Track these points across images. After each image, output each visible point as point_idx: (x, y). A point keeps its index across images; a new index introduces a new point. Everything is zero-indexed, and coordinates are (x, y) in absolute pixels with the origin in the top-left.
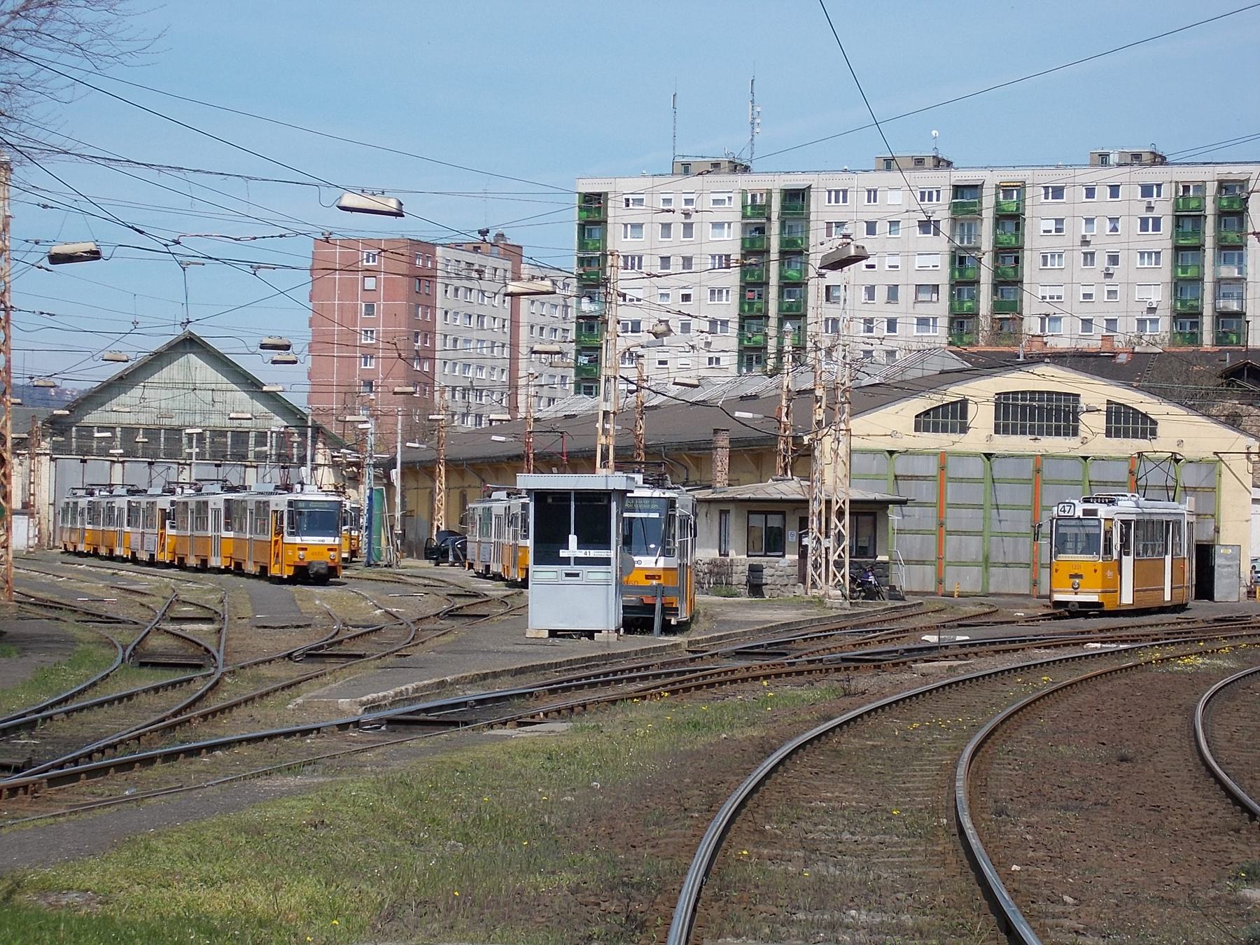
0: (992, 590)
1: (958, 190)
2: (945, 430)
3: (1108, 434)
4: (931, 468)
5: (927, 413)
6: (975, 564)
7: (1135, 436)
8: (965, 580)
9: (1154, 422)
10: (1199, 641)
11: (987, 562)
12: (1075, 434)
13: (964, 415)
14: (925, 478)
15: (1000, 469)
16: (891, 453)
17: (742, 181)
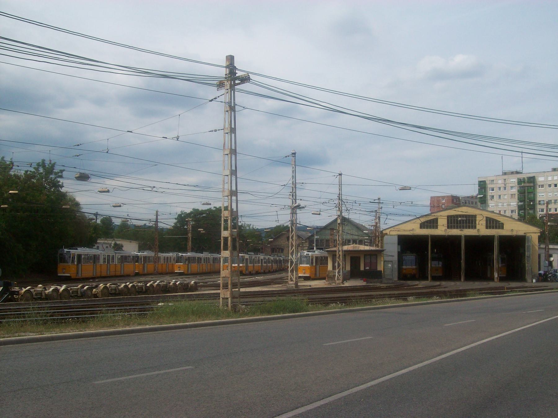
3: (487, 228)
7: (496, 228)
9: (503, 224)
12: (475, 228)
13: (437, 222)
17: (520, 176)
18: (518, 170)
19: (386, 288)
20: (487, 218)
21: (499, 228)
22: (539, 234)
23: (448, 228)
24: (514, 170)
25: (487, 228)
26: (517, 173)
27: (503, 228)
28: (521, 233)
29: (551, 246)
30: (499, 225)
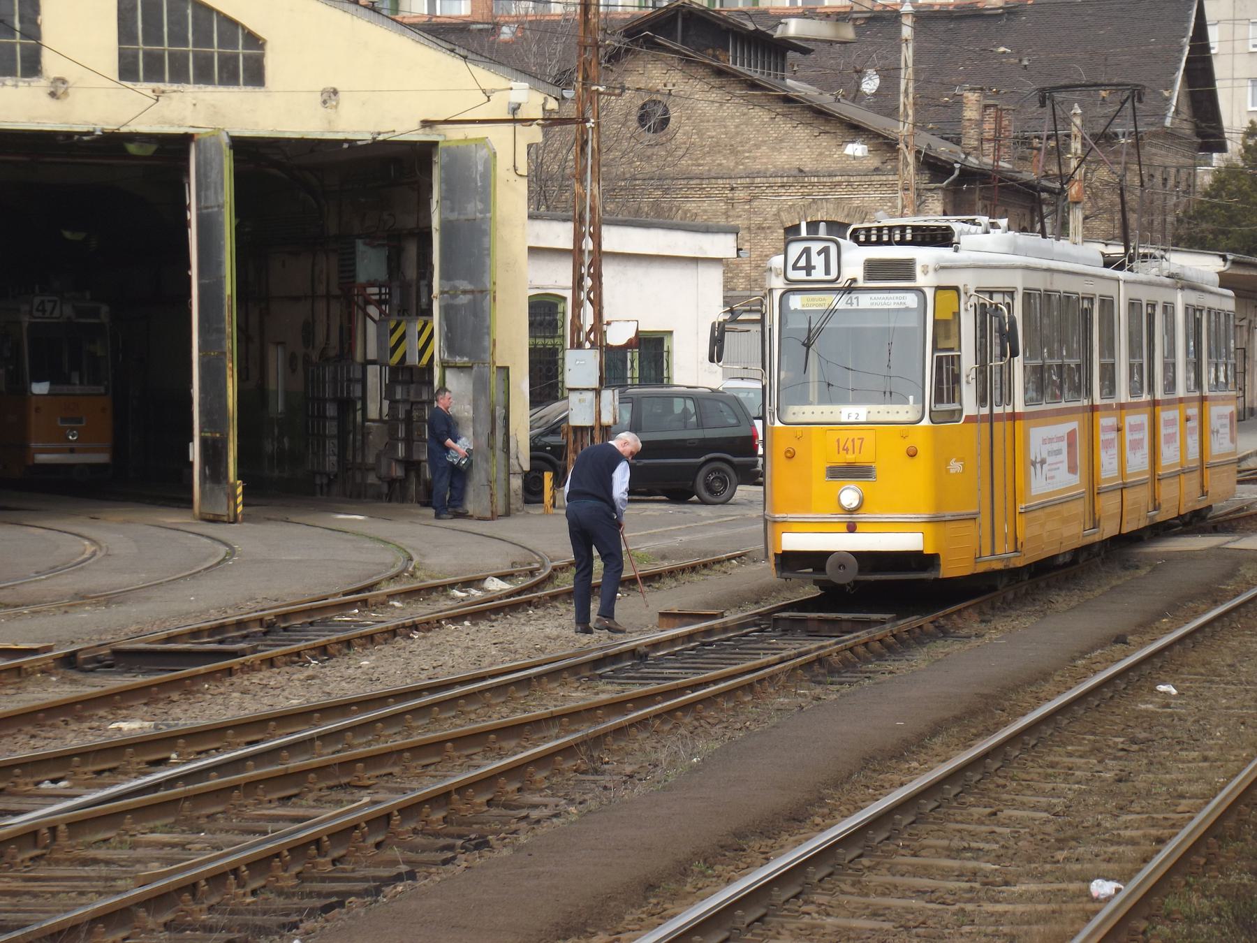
3: (127, 71)
7: (204, 76)
9: (254, 41)
10: (855, 130)
12: (32, 67)
19: (682, 871)
21: (229, 78)
22: (535, 134)
27: (256, 76)
29: (615, 239)
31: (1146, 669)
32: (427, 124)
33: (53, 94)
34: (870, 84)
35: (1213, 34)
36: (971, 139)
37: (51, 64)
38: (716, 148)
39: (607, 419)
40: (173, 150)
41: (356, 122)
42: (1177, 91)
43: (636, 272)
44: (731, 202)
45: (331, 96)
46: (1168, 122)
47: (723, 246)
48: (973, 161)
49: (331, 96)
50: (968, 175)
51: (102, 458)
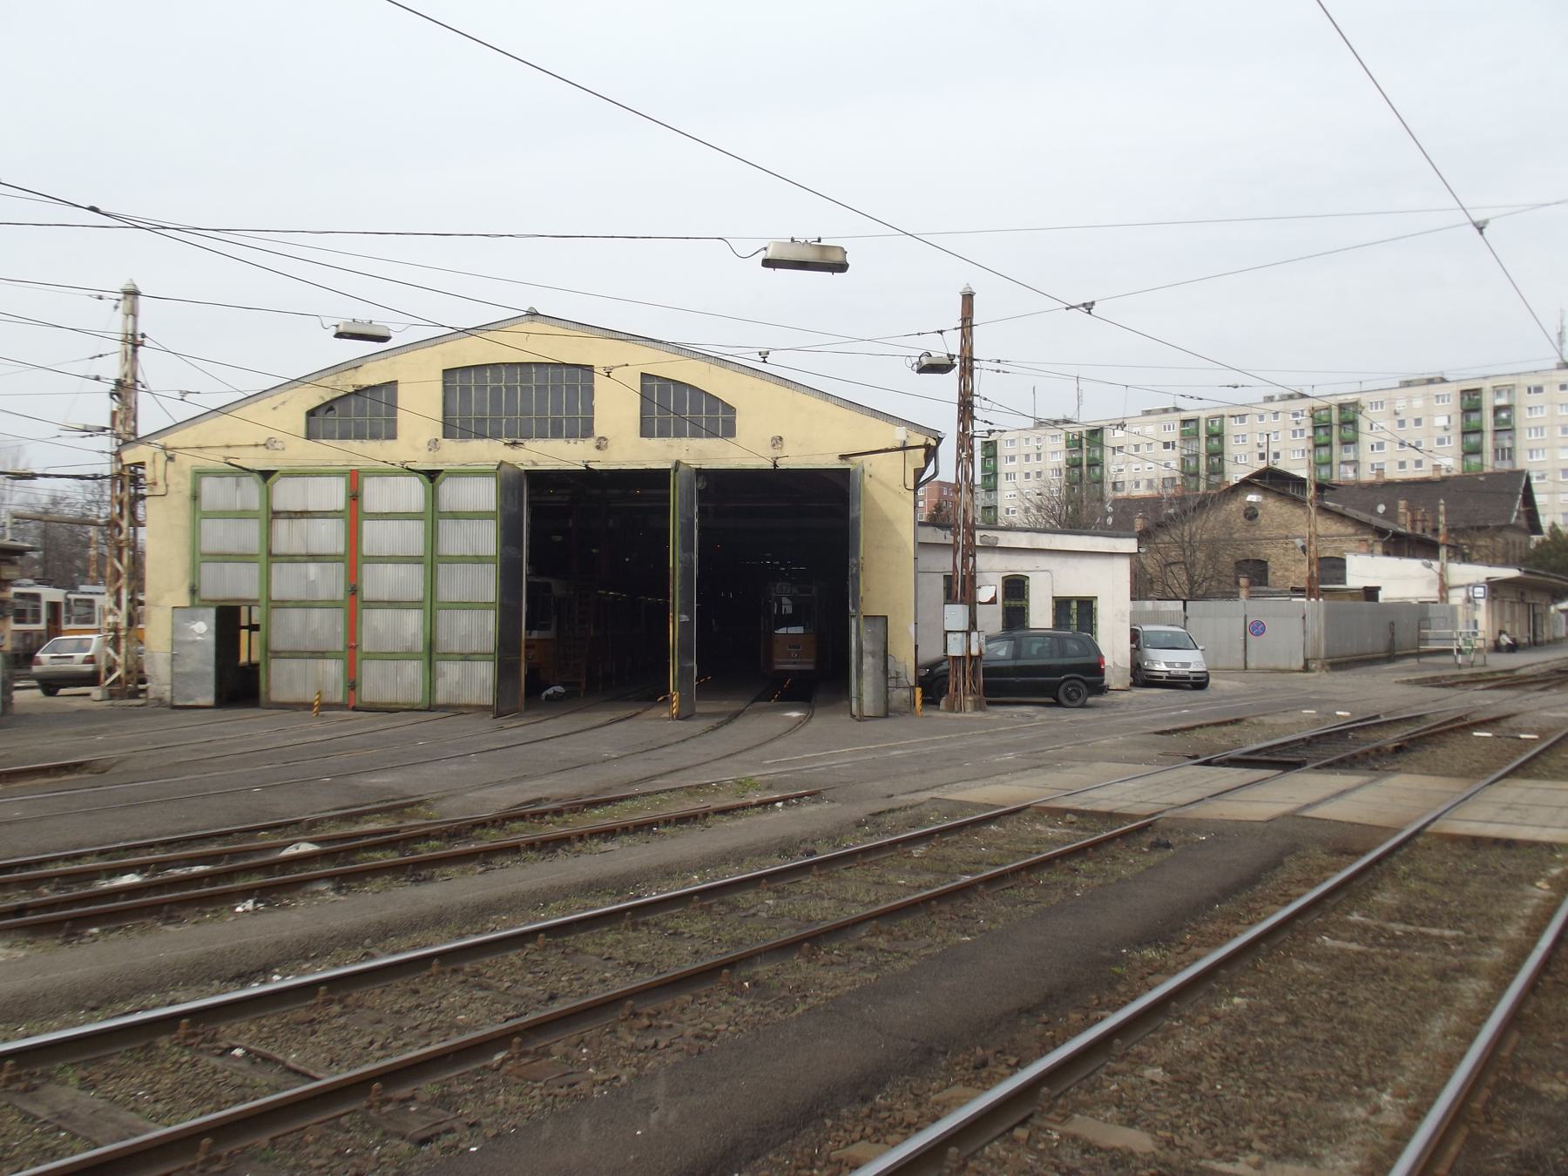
0: (441, 698)
1: (1185, 422)
2: (360, 436)
3: (646, 432)
4: (333, 494)
5: (328, 407)
6: (408, 655)
8: (405, 683)
9: (730, 410)
11: (432, 653)
12: (588, 432)
14: (324, 515)
15: (456, 494)
16: (266, 475)
18: (1069, 416)
20: (645, 376)
23: (447, 434)
24: (1060, 417)
25: (646, 432)
26: (1067, 422)
27: (729, 431)
28: (826, 460)
30: (717, 418)
31: (1330, 902)
32: (843, 457)
33: (598, 447)
34: (1381, 508)
35: (1539, 499)
36: (1402, 520)
37: (598, 432)
38: (1279, 526)
39: (975, 652)
40: (656, 479)
41: (793, 459)
42: (1518, 505)
43: (402, 507)
44: (1286, 550)
45: (778, 441)
46: (1513, 520)
47: (1130, 545)
48: (1401, 530)
49: (778, 441)
50: (1397, 535)
51: (810, 667)
